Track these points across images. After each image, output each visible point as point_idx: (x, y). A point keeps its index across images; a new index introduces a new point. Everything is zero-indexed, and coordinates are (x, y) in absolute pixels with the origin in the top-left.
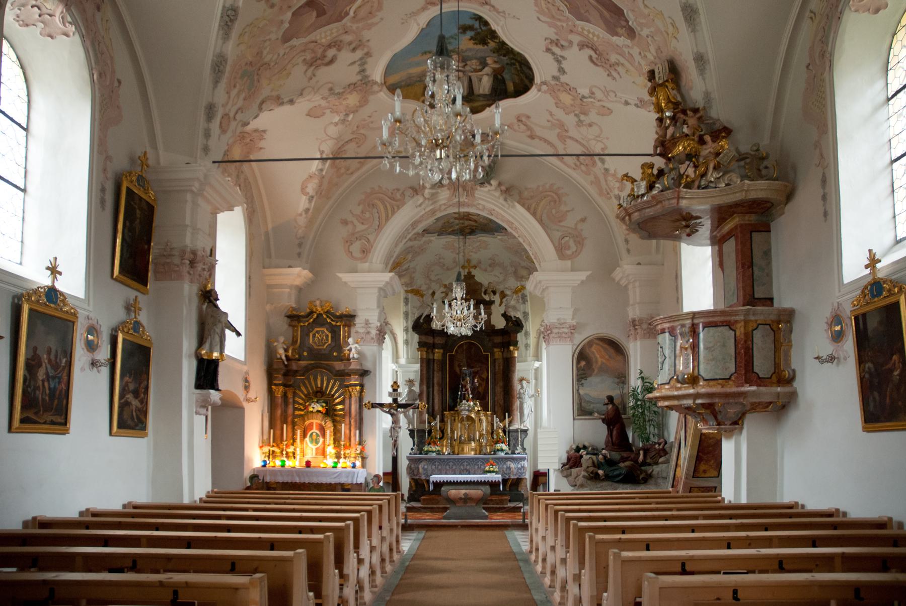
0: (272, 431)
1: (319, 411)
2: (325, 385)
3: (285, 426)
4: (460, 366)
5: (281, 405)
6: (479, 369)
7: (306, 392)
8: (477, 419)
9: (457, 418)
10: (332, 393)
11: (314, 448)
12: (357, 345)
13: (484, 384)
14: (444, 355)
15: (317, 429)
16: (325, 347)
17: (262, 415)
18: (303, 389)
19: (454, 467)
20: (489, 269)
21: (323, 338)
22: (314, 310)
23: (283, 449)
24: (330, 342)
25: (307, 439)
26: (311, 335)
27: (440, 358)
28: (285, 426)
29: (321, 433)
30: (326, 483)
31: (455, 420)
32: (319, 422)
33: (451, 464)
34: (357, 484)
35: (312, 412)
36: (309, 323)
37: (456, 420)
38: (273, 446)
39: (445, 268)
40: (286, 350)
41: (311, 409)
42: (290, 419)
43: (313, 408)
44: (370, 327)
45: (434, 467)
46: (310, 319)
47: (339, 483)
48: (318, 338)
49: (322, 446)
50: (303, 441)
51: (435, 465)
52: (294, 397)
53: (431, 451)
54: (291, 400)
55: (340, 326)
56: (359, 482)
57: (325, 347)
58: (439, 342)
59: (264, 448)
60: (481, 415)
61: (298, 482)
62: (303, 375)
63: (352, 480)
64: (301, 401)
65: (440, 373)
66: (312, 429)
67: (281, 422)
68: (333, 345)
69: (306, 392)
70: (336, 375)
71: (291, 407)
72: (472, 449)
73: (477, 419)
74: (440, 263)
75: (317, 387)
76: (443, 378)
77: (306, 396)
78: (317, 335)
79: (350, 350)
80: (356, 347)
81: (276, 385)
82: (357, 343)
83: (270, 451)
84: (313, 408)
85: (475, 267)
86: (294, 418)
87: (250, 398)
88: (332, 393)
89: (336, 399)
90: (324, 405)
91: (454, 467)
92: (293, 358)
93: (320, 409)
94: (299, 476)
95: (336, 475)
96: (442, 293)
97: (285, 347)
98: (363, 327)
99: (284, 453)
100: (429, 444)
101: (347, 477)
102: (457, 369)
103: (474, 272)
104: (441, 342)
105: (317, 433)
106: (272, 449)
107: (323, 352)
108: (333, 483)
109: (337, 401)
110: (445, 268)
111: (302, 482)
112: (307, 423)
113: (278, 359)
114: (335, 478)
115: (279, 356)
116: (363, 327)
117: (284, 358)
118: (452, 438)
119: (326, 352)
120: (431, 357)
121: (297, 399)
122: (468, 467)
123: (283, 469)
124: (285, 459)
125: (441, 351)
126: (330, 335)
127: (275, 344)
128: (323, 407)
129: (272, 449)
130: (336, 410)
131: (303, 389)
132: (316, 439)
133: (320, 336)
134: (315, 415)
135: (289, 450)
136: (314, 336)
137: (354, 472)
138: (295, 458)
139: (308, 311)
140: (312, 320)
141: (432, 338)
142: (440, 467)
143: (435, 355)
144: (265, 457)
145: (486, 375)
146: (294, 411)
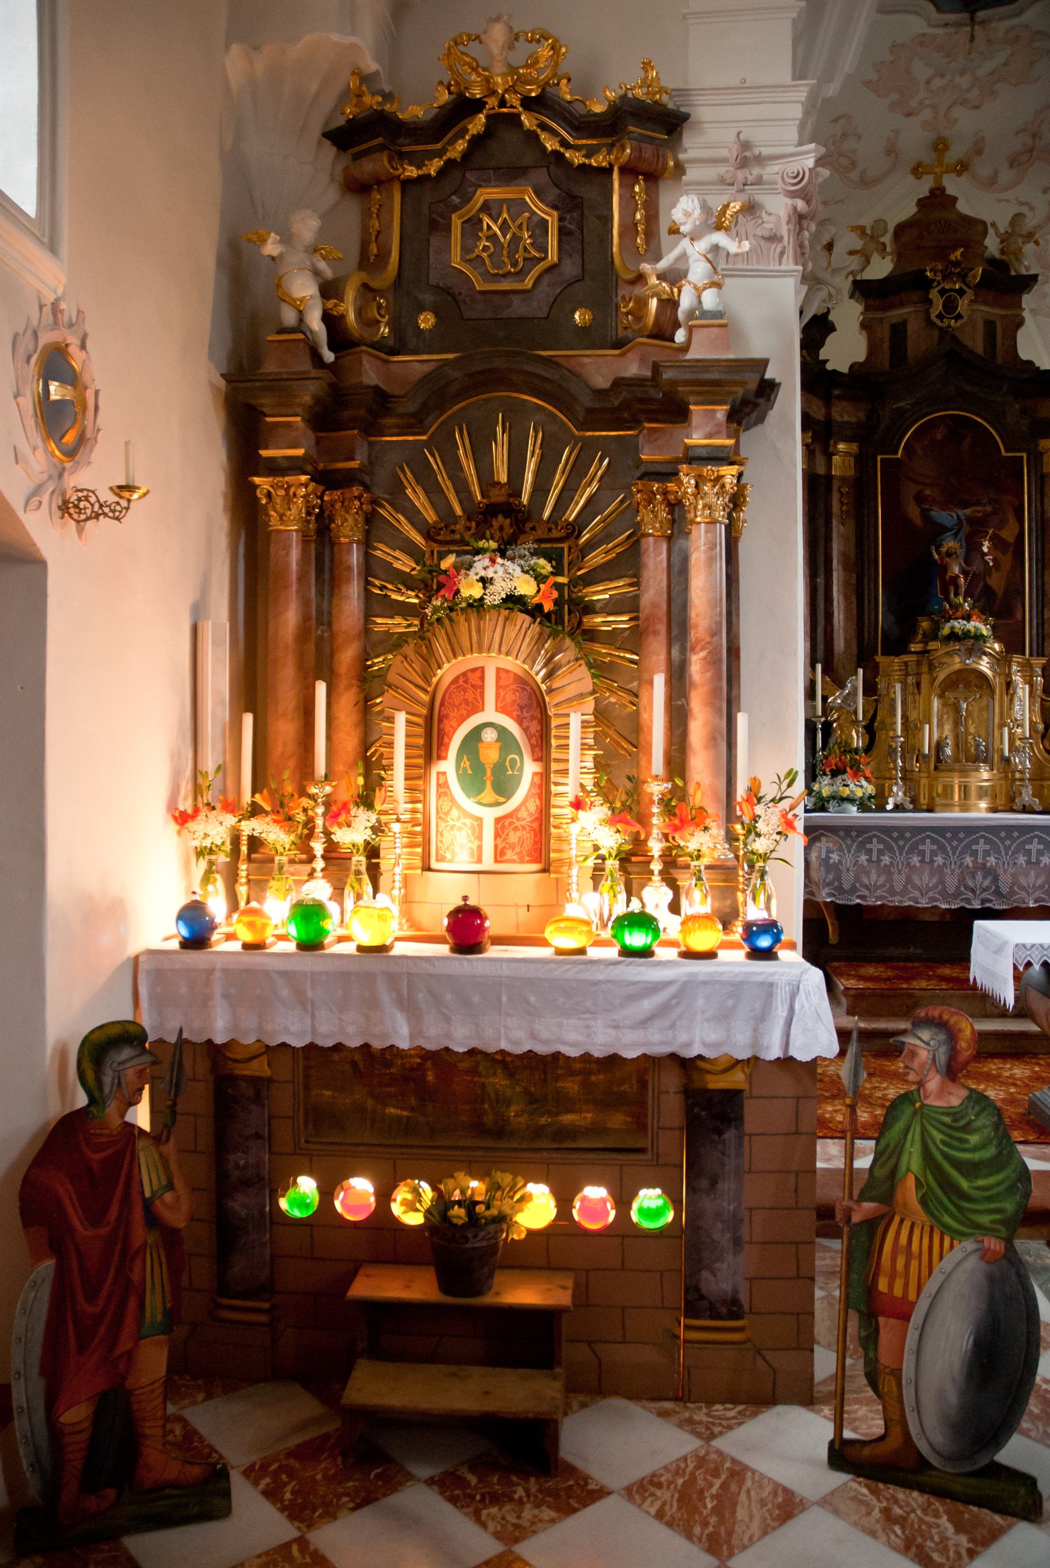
0: (248, 719)
1: (513, 601)
2: (529, 477)
3: (321, 689)
4: (919, 499)
5: (302, 579)
6: (989, 509)
7: (430, 516)
8: (997, 682)
9: (925, 679)
10: (572, 515)
11: (488, 816)
12: (719, 238)
13: (1007, 561)
14: (862, 461)
15: (501, 709)
16: (528, 282)
17: (195, 630)
18: (418, 498)
19: (939, 860)
20: (1006, 175)
21: (516, 239)
22: (477, 93)
23: (309, 823)
24: (553, 255)
25: (448, 766)
26: (456, 222)
27: (851, 472)
28: (321, 689)
29: (529, 736)
30: (586, 1057)
31: (918, 685)
32: (512, 664)
33: (928, 847)
34: (787, 1062)
35: (477, 605)
36: (451, 163)
37: (924, 686)
38: (255, 811)
39: (855, 175)
40: (329, 290)
41: (471, 590)
42: (347, 656)
43: (485, 581)
44: (759, 181)
45: (863, 858)
46: (452, 142)
47: (673, 1056)
48: (492, 238)
49: (533, 806)
50: (425, 777)
51: (869, 852)
52: (367, 544)
53: (843, 800)
54: (355, 558)
55: (609, 171)
56: (802, 1054)
57: (528, 282)
58: (846, 418)
59: (198, 826)
60: (1014, 668)
61: (404, 1044)
62: (415, 423)
63: (755, 1043)
64: (404, 564)
65: (851, 524)
66: (477, 706)
67: (301, 666)
68: (570, 269)
69: (430, 516)
70: (593, 419)
71: (353, 591)
72: (982, 793)
73: (997, 682)
74: (842, 154)
75: (488, 482)
76: (862, 539)
77: (429, 534)
78: (486, 220)
79: (675, 276)
80: (716, 248)
81: (274, 468)
82: (719, 227)
83: (236, 840)
84: (485, 581)
85: (962, 168)
86: (365, 656)
87: (86, 494)
88: (572, 515)
89: (592, 546)
90: (545, 566)
91: (939, 860)
92: (367, 334)
93: (526, 587)
94: (408, 1006)
95: (647, 1005)
96: (851, 253)
97: (329, 273)
98: (724, 182)
99: (318, 847)
100: (835, 774)
101: (724, 1017)
102: (913, 512)
103: (952, 185)
104: (853, 420)
105: (502, 731)
106: (248, 827)
107: (519, 308)
108: (630, 1054)
109: (596, 558)
110: (855, 175)
111: (432, 1046)
112: (447, 672)
113: (283, 330)
114: (644, 1023)
115: (289, 317)
116: (722, 181)
117: (315, 323)
118: (911, 750)
119: (537, 307)
120: (821, 470)
121: (382, 551)
122: (992, 860)
123: (309, 962)
124: (319, 889)
125: (854, 447)
126: (552, 219)
127: (271, 248)
128: (540, 579)
129: (248, 827)
130: (589, 609)
131: (418, 498)
132: (499, 768)
133: (504, 228)
134: (492, 626)
135: (344, 837)
136: (473, 224)
137: (768, 988)
138: (374, 872)
139: (445, 97)
140: (461, 146)
141: (820, 403)
142: (886, 859)
143: (836, 459)
144: (207, 878)
145: (1017, 531)
146: (368, 615)
